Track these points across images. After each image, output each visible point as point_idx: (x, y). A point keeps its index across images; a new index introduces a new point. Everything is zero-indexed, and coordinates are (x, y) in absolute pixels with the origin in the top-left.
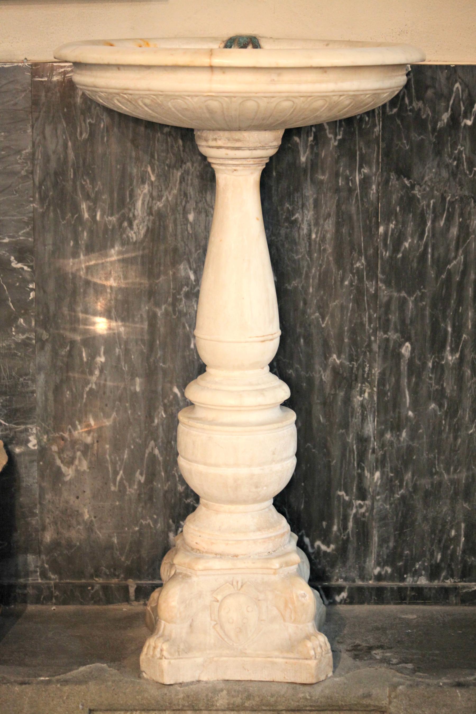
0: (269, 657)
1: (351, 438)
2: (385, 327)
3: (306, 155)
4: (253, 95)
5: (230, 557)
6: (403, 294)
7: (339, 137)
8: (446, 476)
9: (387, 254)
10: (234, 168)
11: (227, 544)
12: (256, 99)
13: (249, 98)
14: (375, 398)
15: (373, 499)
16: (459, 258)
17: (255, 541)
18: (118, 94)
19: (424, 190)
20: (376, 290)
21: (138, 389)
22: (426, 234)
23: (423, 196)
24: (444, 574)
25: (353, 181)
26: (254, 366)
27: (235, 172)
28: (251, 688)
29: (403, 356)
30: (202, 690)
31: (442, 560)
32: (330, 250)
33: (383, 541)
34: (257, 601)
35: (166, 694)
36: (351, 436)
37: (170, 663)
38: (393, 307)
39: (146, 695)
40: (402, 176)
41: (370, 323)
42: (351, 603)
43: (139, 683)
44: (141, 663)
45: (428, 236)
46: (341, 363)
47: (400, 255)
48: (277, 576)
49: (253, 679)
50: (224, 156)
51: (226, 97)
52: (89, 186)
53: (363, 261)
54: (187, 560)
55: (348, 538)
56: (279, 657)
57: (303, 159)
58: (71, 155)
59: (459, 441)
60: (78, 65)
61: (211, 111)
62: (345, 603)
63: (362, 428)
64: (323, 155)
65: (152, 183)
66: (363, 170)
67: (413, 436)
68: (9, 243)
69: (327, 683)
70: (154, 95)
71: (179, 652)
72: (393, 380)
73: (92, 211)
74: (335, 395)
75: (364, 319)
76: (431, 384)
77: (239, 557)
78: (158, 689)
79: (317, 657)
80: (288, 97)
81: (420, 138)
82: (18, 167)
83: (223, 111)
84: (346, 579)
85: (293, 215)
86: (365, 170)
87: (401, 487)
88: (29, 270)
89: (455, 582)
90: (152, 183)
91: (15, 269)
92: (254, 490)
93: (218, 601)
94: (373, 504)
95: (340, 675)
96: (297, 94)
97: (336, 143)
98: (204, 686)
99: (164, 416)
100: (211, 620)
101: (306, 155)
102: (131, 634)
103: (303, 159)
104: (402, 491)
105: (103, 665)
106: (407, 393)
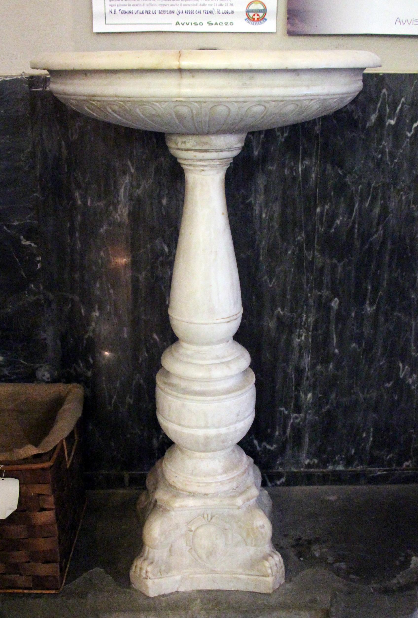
1: (290, 370)
2: (319, 285)
3: (258, 150)
4: (225, 99)
6: (335, 261)
7: (285, 135)
8: (361, 395)
9: (323, 230)
10: (202, 168)
12: (226, 104)
13: (219, 104)
14: (310, 340)
15: (306, 413)
16: (379, 232)
17: (222, 483)
18: (87, 101)
19: (354, 178)
20: (313, 258)
21: (126, 336)
22: (354, 214)
23: (352, 183)
24: (356, 463)
25: (297, 172)
26: (220, 342)
27: (203, 172)
29: (333, 308)
31: (355, 453)
32: (277, 227)
33: (312, 442)
36: (291, 368)
38: (326, 271)
40: (337, 167)
41: (308, 282)
42: (288, 485)
45: (356, 215)
46: (284, 314)
47: (333, 230)
48: (240, 510)
50: (192, 157)
51: (196, 102)
52: (80, 177)
53: (303, 235)
55: (287, 440)
56: (242, 574)
57: (256, 153)
58: (65, 152)
59: (372, 371)
60: (56, 73)
61: (180, 117)
62: (283, 486)
63: (299, 362)
64: (272, 150)
65: (132, 175)
66: (304, 162)
67: (337, 368)
68: (19, 225)
70: (122, 101)
72: (324, 326)
73: (84, 198)
74: (279, 339)
75: (303, 281)
76: (354, 329)
79: (273, 574)
80: (259, 101)
81: (352, 135)
82: (22, 163)
83: (193, 117)
85: (247, 199)
86: (307, 162)
87: (327, 403)
88: (35, 246)
89: (364, 468)
90: (132, 175)
91: (24, 245)
92: (221, 444)
93: (191, 531)
94: (306, 417)
96: (269, 99)
97: (283, 140)
99: (147, 355)
100: (187, 545)
101: (258, 150)
103: (256, 153)
104: (328, 407)
106: (334, 336)
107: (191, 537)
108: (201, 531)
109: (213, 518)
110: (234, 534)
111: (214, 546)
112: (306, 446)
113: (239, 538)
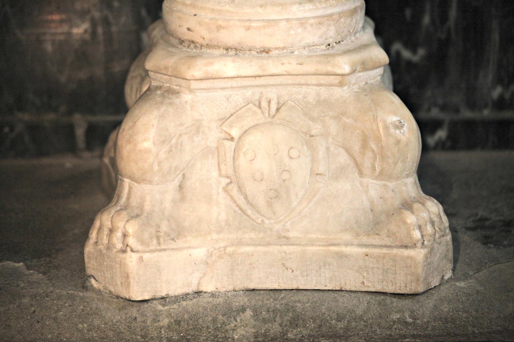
0: (332, 245)
5: (253, 53)
11: (248, 28)
17: (302, 22)
28: (299, 305)
30: (205, 309)
34: (309, 138)
35: (136, 318)
37: (141, 259)
39: (97, 322)
43: (82, 298)
44: (86, 260)
48: (345, 88)
49: (301, 287)
54: (171, 62)
56: (352, 245)
69: (444, 291)
71: (158, 238)
77: (271, 54)
78: (119, 310)
84: (443, 108)
93: (232, 139)
95: (466, 277)
98: (209, 303)
100: (220, 175)
102: (76, 207)
105: (16, 265)
107: (230, 155)
108: (255, 139)
109: (283, 108)
110: (332, 149)
111: (285, 176)
112: (493, 54)
113: (343, 158)
